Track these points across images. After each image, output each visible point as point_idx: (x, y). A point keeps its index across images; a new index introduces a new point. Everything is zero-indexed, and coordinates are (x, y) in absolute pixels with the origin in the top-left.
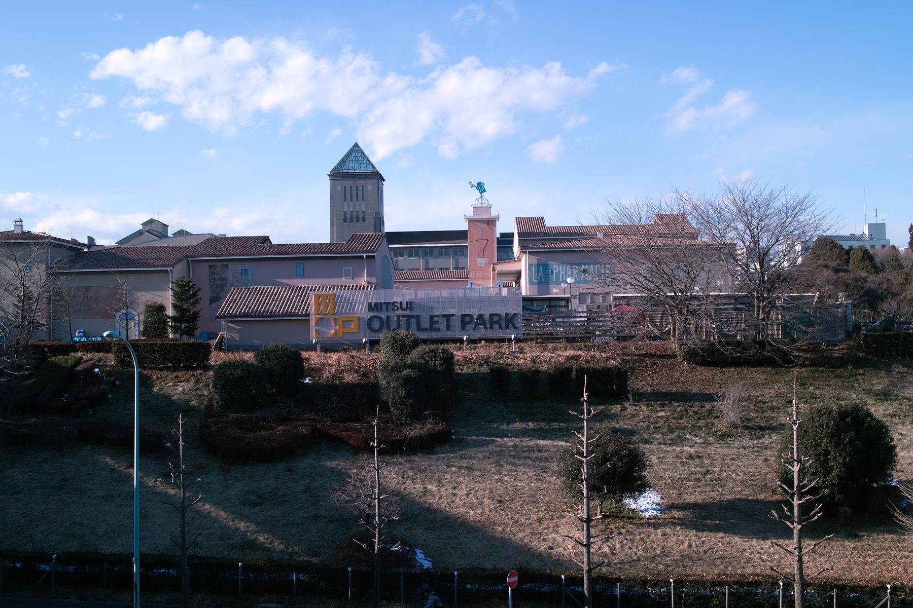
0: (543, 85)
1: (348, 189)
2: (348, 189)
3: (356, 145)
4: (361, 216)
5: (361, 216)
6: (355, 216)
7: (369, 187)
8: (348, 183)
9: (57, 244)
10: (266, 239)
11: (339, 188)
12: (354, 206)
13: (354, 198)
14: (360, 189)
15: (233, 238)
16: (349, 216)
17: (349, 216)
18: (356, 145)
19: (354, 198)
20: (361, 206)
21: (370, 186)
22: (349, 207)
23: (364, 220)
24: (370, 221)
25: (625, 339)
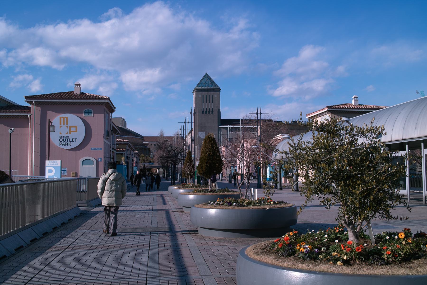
0: (318, 50)
1: (205, 97)
2: (205, 97)
3: (206, 74)
4: (211, 110)
5: (211, 110)
6: (208, 111)
7: (216, 96)
8: (205, 93)
9: (287, 124)
10: (271, 120)
11: (200, 96)
12: (208, 105)
13: (208, 101)
14: (211, 97)
15: (21, 106)
16: (205, 110)
17: (205, 110)
18: (206, 74)
19: (208, 101)
20: (211, 106)
21: (215, 95)
22: (205, 106)
23: (212, 113)
24: (216, 113)
25: (369, 195)
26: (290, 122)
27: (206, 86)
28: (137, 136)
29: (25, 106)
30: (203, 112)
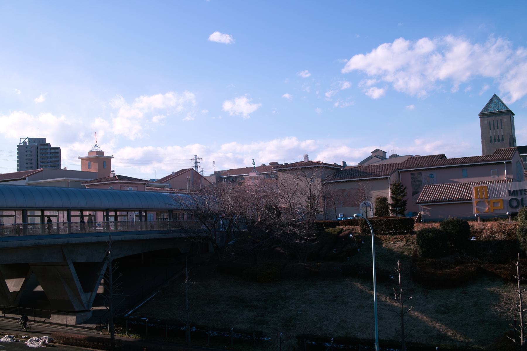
1: (492, 122)
2: (492, 122)
3: (495, 95)
5: (500, 138)
6: (497, 138)
8: (491, 119)
11: (486, 122)
13: (496, 128)
14: (499, 122)
15: (424, 157)
16: (493, 139)
17: (493, 139)
18: (495, 95)
19: (496, 128)
20: (500, 132)
21: (505, 119)
23: (503, 140)
26: (267, 165)
27: (492, 110)
28: (312, 164)
29: (183, 170)
30: (491, 141)
